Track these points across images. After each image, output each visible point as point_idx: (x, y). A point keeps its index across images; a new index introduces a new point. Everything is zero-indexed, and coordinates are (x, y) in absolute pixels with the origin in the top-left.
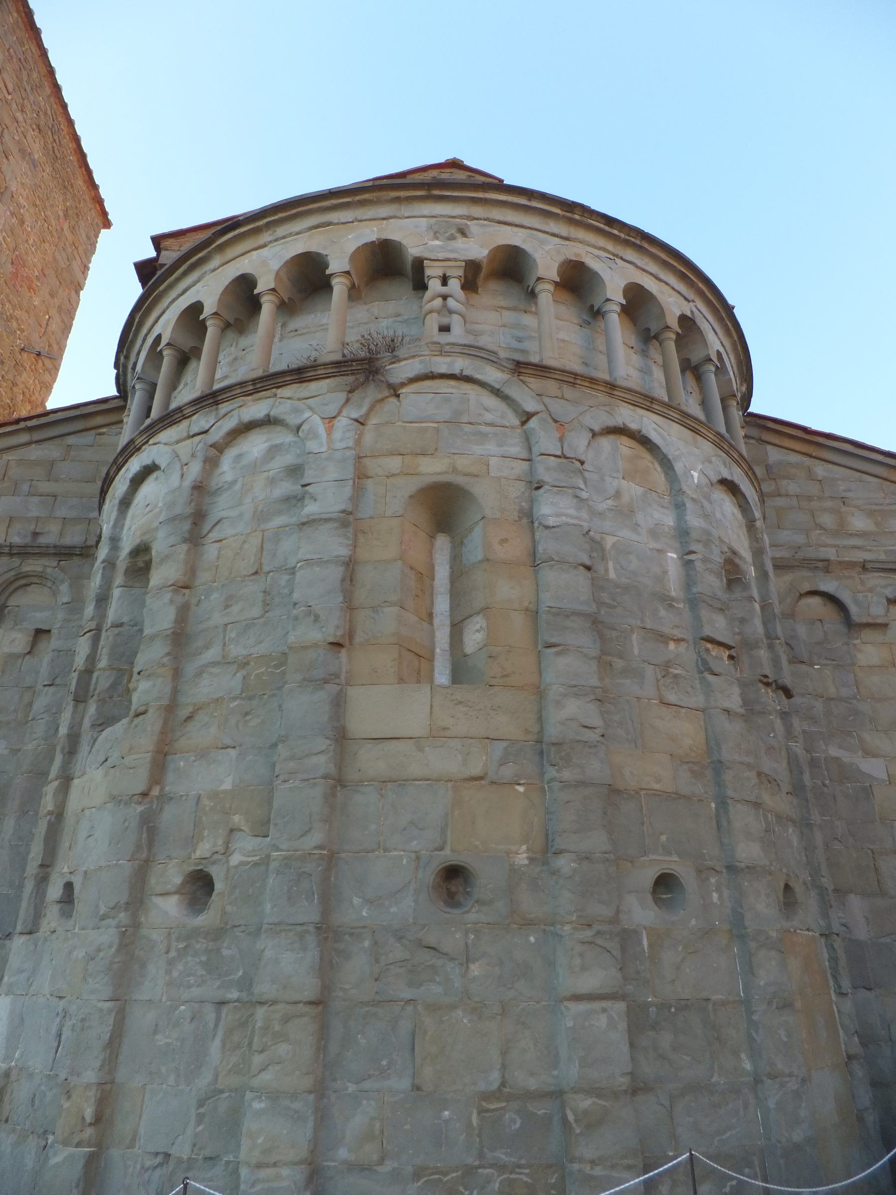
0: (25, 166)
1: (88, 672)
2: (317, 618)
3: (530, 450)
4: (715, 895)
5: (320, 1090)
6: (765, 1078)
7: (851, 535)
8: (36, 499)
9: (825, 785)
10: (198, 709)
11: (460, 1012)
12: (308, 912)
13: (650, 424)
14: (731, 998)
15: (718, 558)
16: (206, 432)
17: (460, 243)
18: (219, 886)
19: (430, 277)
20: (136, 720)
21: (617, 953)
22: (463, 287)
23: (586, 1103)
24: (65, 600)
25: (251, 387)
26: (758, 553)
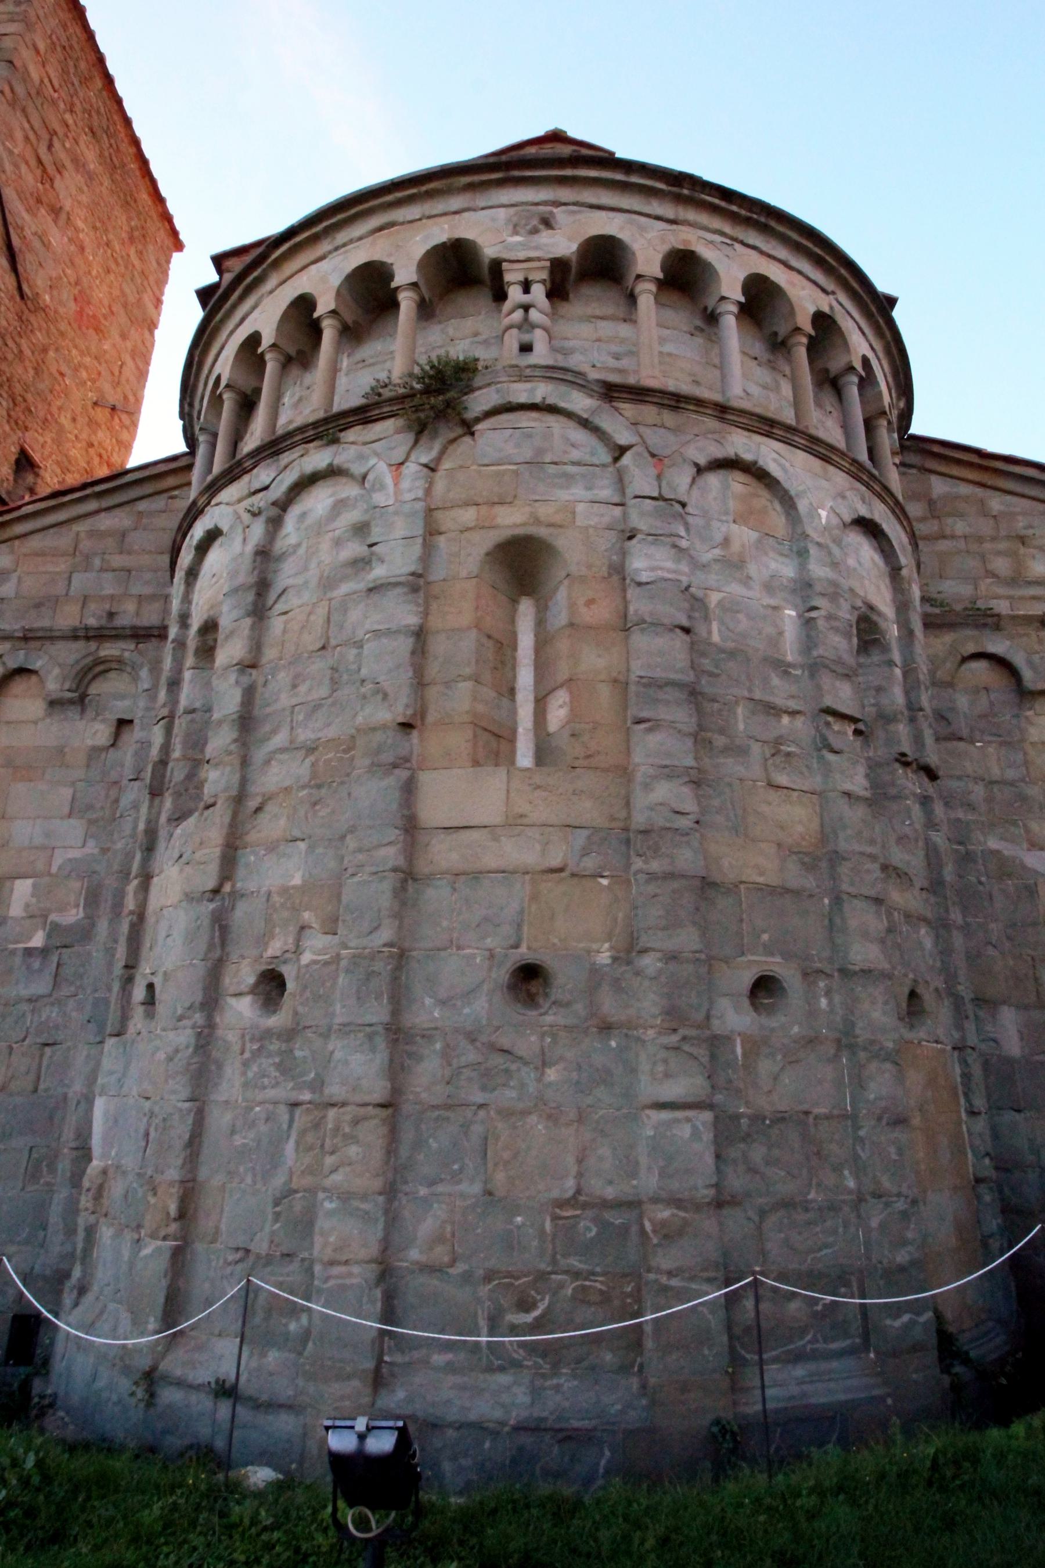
0: (79, 179)
1: (163, 762)
2: (385, 696)
3: (622, 491)
4: (823, 1002)
5: (390, 1192)
6: (868, 1197)
7: (1030, 583)
8: (109, 575)
9: (980, 883)
10: (267, 798)
11: (533, 1119)
12: (377, 1013)
13: (768, 453)
14: (836, 1112)
15: (846, 614)
16: (266, 488)
17: (545, 237)
18: (290, 985)
19: (510, 284)
20: (207, 813)
21: (705, 1060)
22: (550, 295)
23: (665, 1213)
24: (146, 686)
25: (311, 433)
26: (902, 607)
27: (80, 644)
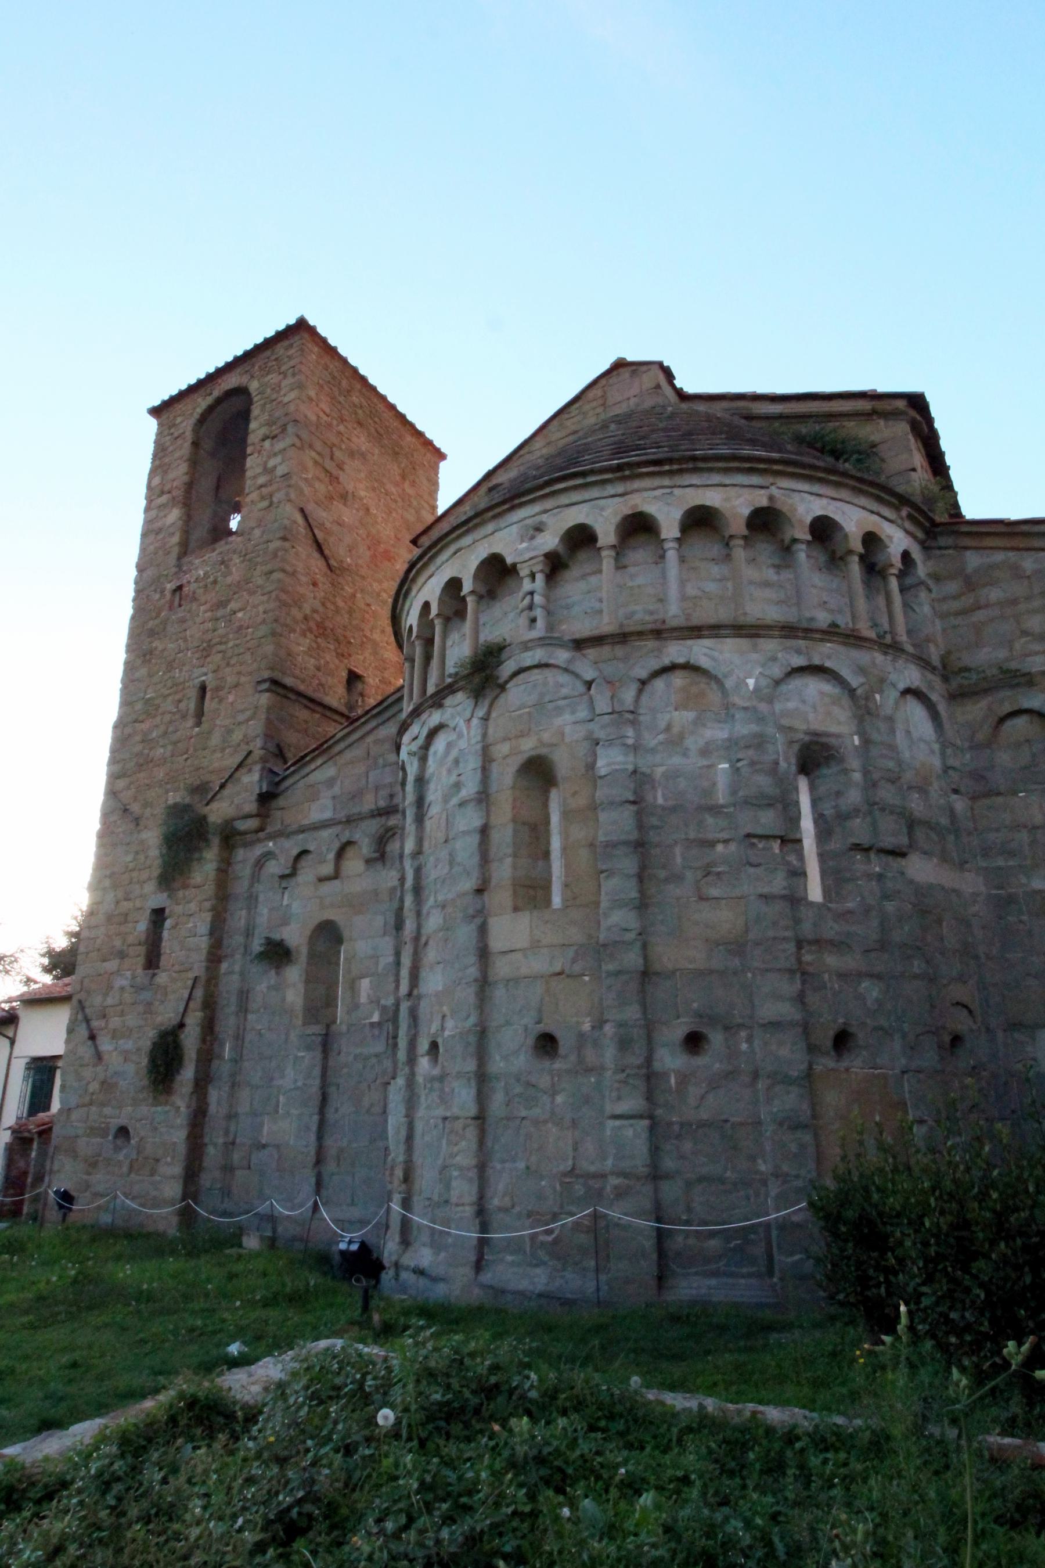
11: (550, 1125)
27: (378, 819)
